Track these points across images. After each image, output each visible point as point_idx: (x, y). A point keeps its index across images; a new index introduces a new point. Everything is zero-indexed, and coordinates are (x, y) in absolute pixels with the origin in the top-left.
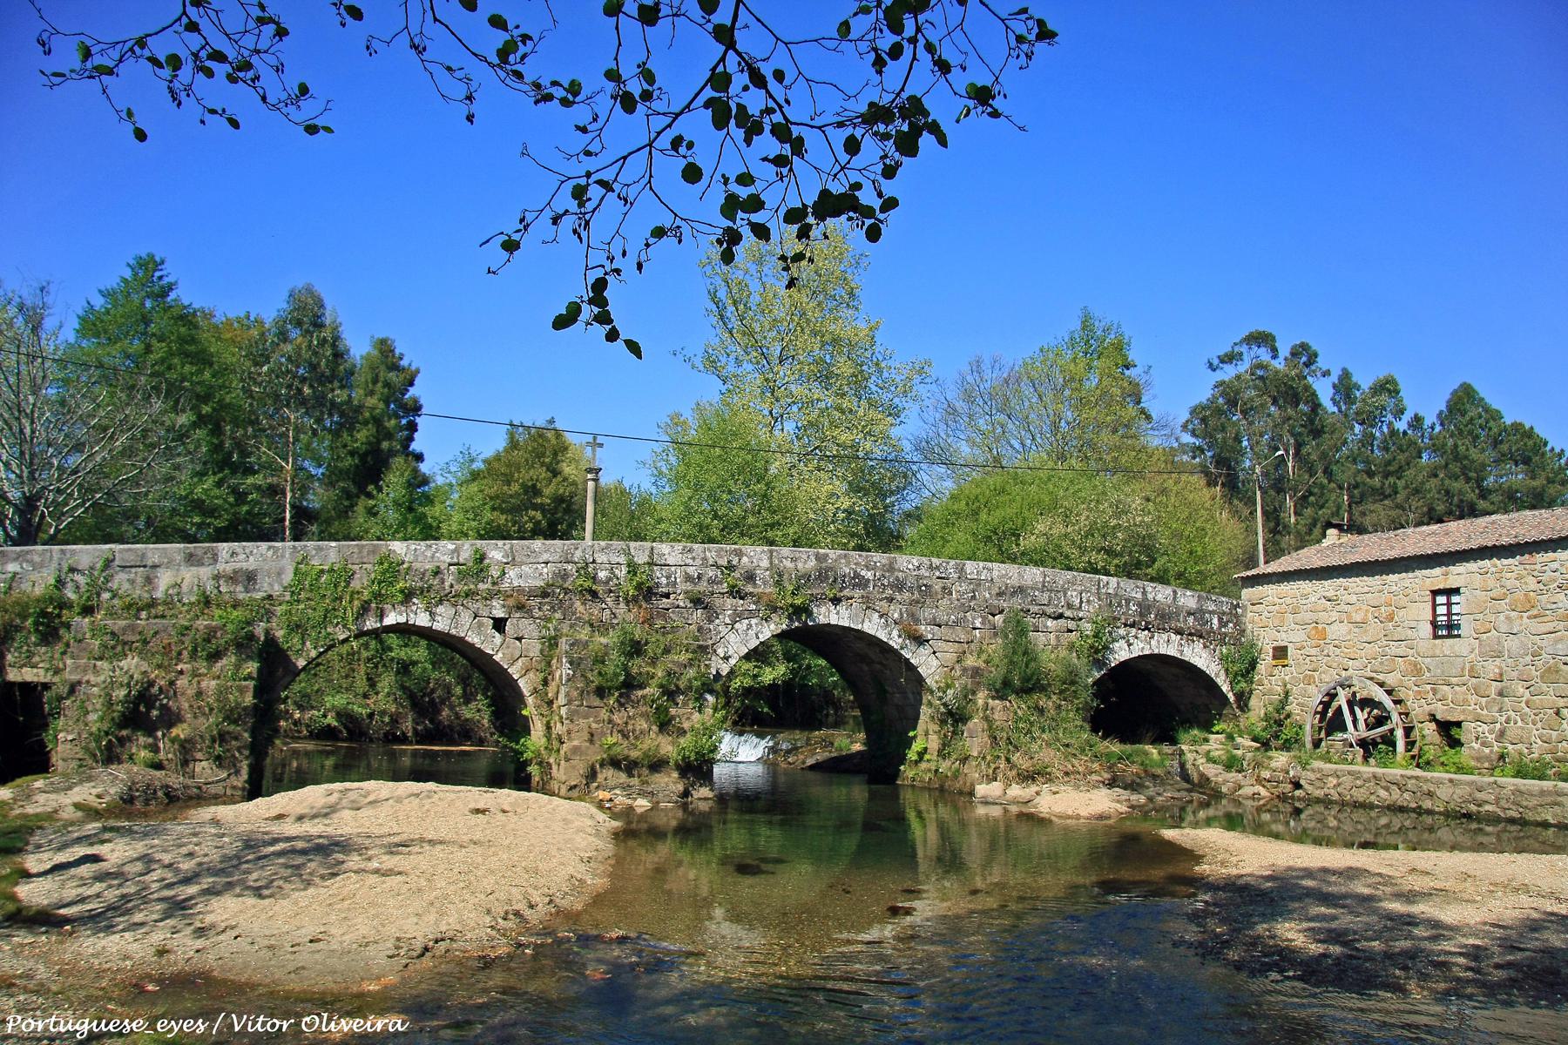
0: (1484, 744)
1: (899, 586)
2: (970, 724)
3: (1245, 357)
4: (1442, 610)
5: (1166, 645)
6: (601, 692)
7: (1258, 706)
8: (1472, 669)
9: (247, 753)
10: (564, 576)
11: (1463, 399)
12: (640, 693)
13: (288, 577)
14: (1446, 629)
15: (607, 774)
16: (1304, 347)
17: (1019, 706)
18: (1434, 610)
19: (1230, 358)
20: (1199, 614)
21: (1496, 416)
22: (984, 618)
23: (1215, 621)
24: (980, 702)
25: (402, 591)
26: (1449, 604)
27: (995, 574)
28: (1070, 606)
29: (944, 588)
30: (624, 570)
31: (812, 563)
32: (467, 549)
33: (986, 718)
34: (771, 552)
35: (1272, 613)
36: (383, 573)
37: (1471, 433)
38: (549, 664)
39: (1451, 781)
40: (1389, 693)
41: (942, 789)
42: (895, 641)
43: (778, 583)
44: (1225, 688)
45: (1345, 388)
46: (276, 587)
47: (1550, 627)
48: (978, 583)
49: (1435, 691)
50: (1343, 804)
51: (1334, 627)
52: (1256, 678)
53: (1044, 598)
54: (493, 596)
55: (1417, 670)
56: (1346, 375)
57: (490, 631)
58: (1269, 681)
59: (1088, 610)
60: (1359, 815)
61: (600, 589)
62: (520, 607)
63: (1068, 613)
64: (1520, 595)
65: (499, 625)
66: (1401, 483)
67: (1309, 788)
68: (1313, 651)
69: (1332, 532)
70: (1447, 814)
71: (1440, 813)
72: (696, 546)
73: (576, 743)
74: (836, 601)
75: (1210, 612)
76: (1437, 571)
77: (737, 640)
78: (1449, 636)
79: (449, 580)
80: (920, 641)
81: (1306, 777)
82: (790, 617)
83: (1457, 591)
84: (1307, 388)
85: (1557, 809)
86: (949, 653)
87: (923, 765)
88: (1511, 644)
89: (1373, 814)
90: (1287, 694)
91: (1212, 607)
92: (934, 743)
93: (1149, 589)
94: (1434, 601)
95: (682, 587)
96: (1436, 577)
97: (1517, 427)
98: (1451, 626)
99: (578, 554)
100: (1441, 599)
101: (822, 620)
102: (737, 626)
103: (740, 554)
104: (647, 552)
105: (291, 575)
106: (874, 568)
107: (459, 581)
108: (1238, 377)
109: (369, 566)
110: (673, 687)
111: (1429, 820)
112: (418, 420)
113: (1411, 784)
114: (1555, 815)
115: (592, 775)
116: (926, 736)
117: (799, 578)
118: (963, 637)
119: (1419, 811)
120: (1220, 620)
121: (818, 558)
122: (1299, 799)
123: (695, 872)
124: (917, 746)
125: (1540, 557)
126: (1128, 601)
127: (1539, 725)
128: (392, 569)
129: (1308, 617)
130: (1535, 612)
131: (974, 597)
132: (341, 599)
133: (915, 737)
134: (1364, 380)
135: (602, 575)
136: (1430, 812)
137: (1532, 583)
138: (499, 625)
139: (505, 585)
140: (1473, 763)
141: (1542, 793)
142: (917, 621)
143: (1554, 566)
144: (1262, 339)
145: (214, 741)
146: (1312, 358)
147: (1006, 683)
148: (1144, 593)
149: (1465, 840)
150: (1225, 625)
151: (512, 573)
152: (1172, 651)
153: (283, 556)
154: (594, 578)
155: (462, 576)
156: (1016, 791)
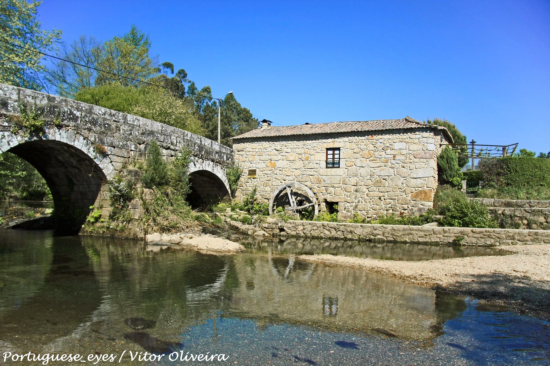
0: (347, 211)
1: (94, 122)
2: (133, 202)
4: (330, 156)
5: (208, 166)
7: (240, 198)
14: (333, 164)
21: (239, 105)
22: (136, 145)
23: (225, 157)
24: (139, 190)
26: (334, 154)
27: (141, 123)
28: (172, 144)
29: (117, 127)
31: (45, 102)
34: (19, 90)
37: (231, 109)
39: (361, 226)
41: (113, 237)
42: (92, 154)
44: (228, 187)
45: (192, 89)
47: (378, 165)
50: (306, 237)
53: (162, 138)
59: (180, 147)
60: (315, 242)
63: (172, 147)
66: (211, 123)
67: (289, 231)
68: (269, 172)
70: (360, 240)
71: (356, 240)
74: (59, 127)
75: (224, 153)
76: (330, 140)
78: (333, 167)
80: (104, 155)
81: (286, 226)
82: (31, 133)
84: (182, 86)
85: (411, 236)
87: (98, 224)
89: (322, 241)
90: (255, 191)
92: (107, 211)
93: (203, 140)
94: (327, 152)
96: (331, 143)
97: (245, 110)
98: (333, 163)
100: (330, 152)
101: (51, 137)
106: (81, 110)
111: (350, 243)
113: (342, 228)
114: (409, 239)
116: (102, 209)
118: (126, 155)
119: (345, 239)
120: (227, 156)
122: (283, 236)
124: (95, 213)
125: (375, 137)
126: (195, 144)
127: (372, 203)
129: (267, 157)
130: (372, 158)
131: (131, 134)
133: (93, 209)
134: (199, 87)
137: (372, 147)
140: (343, 219)
142: (103, 143)
144: (168, 65)
146: (185, 76)
147: (153, 180)
148: (201, 141)
149: (368, 251)
152: (209, 169)
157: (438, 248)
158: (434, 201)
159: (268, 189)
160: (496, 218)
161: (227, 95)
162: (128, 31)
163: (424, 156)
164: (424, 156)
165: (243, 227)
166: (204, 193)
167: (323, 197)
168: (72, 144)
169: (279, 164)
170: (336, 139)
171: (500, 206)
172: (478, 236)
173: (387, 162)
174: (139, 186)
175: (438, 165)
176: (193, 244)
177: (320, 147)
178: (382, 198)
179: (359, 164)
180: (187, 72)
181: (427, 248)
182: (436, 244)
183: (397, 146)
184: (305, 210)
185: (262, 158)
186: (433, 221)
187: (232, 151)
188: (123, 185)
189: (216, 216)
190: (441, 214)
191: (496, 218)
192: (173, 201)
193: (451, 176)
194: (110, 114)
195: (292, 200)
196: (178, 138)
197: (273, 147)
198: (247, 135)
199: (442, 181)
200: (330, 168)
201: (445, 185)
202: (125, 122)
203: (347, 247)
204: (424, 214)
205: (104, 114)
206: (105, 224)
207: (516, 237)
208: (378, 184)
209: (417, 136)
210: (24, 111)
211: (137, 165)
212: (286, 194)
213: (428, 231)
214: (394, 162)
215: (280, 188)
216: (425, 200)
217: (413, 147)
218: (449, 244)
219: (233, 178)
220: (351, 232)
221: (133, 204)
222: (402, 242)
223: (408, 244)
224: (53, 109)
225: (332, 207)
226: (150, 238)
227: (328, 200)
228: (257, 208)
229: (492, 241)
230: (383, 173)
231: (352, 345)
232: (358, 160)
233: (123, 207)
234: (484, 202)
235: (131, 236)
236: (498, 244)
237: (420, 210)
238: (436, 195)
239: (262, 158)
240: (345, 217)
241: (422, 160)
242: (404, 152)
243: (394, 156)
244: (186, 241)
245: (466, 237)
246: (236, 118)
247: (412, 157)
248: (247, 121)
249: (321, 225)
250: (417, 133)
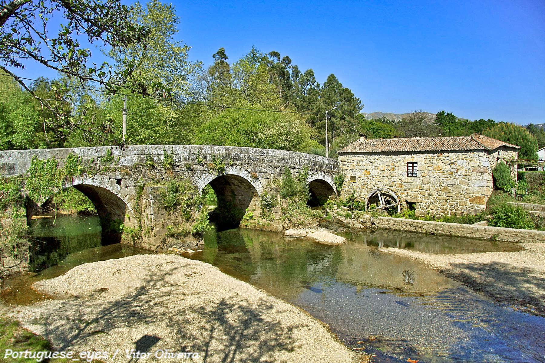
1: (250, 159)
4: (410, 168)
5: (320, 176)
6: (166, 208)
7: (344, 197)
8: (420, 187)
9: (28, 251)
10: (142, 160)
11: (332, 79)
12: (179, 207)
13: (29, 166)
14: (412, 174)
15: (171, 240)
16: (287, 58)
17: (290, 201)
21: (341, 85)
24: (279, 200)
25: (80, 170)
26: (413, 167)
28: (297, 164)
30: (163, 156)
31: (224, 151)
32: (104, 150)
33: (281, 206)
34: (211, 147)
35: (349, 165)
36: (71, 163)
38: (140, 196)
39: (428, 224)
43: (215, 160)
44: (335, 189)
45: (296, 72)
46: (24, 171)
47: (445, 176)
49: (407, 193)
50: (390, 230)
52: (343, 186)
55: (402, 186)
58: (348, 187)
61: (156, 165)
62: (127, 174)
63: (297, 167)
64: (437, 166)
65: (119, 181)
67: (378, 225)
68: (365, 178)
69: (362, 138)
70: (426, 234)
73: (158, 229)
74: (232, 166)
76: (410, 156)
78: (412, 176)
79: (98, 164)
80: (257, 179)
86: (264, 182)
87: (251, 221)
88: (433, 180)
90: (355, 192)
95: (183, 162)
97: (347, 90)
98: (412, 173)
99: (147, 150)
100: (410, 165)
101: (228, 173)
103: (201, 149)
104: (171, 149)
105: (30, 166)
107: (102, 164)
109: (65, 160)
110: (190, 204)
111: (420, 235)
115: (165, 241)
117: (220, 157)
118: (269, 177)
119: (417, 232)
121: (227, 149)
122: (374, 228)
128: (75, 161)
132: (54, 175)
134: (303, 71)
135: (156, 159)
136: (420, 233)
138: (119, 181)
139: (120, 165)
141: (457, 228)
143: (448, 158)
144: (275, 54)
145: (14, 247)
146: (290, 62)
151: (122, 160)
153: (26, 157)
154: (153, 160)
155: (104, 162)
157: (480, 242)
158: (486, 204)
159: (364, 191)
160: (534, 219)
161: (329, 77)
162: (249, 50)
163: (481, 170)
164: (481, 170)
165: (346, 221)
166: (318, 195)
167: (405, 198)
168: (238, 175)
169: (373, 172)
170: (415, 156)
171: (538, 210)
172: (509, 235)
173: (452, 174)
174: (279, 197)
175: (493, 176)
176: (315, 237)
177: (402, 161)
178: (448, 201)
179: (431, 175)
180: (291, 58)
181: (473, 241)
182: (479, 239)
183: (460, 162)
184: (393, 207)
185: (360, 167)
186: (484, 220)
187: (338, 162)
188: (269, 198)
189: (327, 212)
190: (491, 214)
191: (534, 219)
192: (300, 206)
193: (503, 184)
194: (259, 152)
195: (382, 199)
196: (300, 158)
197: (368, 160)
198: (348, 149)
199: (496, 188)
200: (410, 177)
201: (499, 191)
203: (418, 238)
204: (478, 214)
206: (256, 221)
207: (536, 237)
208: (445, 190)
209: (475, 156)
210: (215, 160)
211: (276, 184)
212: (377, 194)
213: (474, 229)
214: (457, 174)
215: (373, 192)
216: (479, 203)
218: (488, 240)
219: (338, 183)
220: (421, 227)
221: (275, 210)
222: (456, 236)
223: (459, 239)
224: (228, 156)
225: (411, 205)
226: (288, 232)
227: (408, 201)
228: (356, 205)
229: (519, 239)
230: (448, 182)
231: (384, 293)
232: (431, 172)
233: (269, 211)
234: (526, 206)
235: (274, 230)
236: (523, 241)
237: (475, 211)
238: (489, 200)
239: (360, 167)
240: (420, 214)
242: (465, 167)
243: (457, 170)
244: (310, 235)
245: (500, 235)
246: (339, 98)
247: (471, 171)
248: (349, 101)
249: (401, 222)
250: (475, 153)
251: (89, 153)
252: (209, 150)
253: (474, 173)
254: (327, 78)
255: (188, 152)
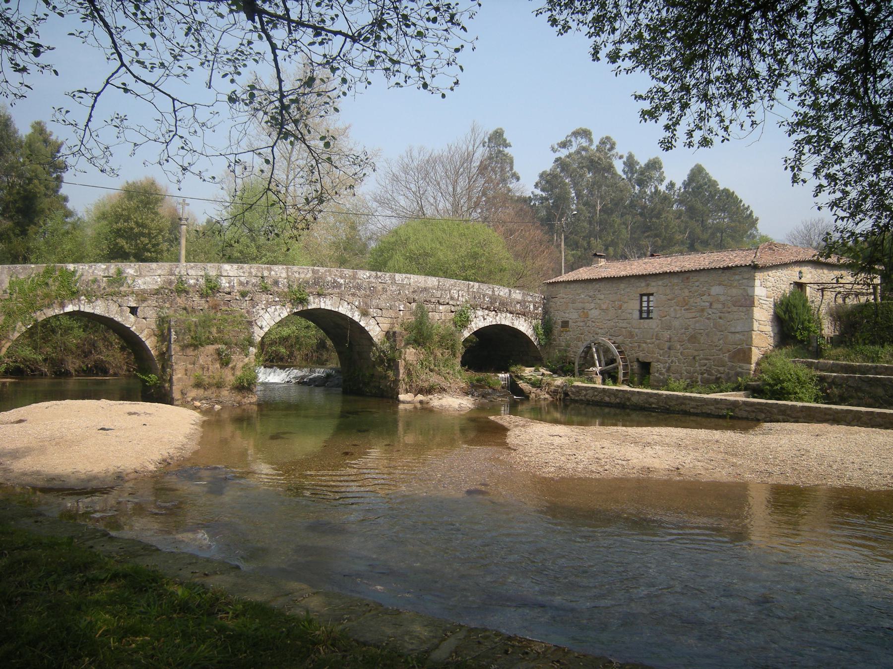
0: (660, 374)
1: (359, 287)
3: (574, 143)
5: (506, 319)
8: (657, 336)
18: (641, 304)
19: (564, 145)
20: (522, 303)
21: (714, 184)
22: (405, 305)
23: (532, 307)
26: (648, 301)
28: (452, 298)
31: (310, 275)
34: (287, 268)
40: (617, 348)
42: (356, 317)
45: (630, 163)
47: (693, 315)
48: (403, 286)
51: (593, 311)
53: (438, 294)
54: (134, 295)
55: (631, 335)
56: (631, 157)
57: (128, 314)
68: (582, 324)
72: (245, 265)
77: (269, 318)
83: (652, 294)
91: (530, 299)
93: (496, 289)
96: (642, 287)
97: (726, 191)
100: (645, 298)
102: (269, 310)
103: (270, 270)
106: (345, 278)
108: (569, 156)
112: (63, 174)
120: (534, 306)
123: (244, 442)
129: (581, 305)
130: (687, 307)
131: (400, 293)
138: (134, 311)
144: (585, 133)
148: (493, 291)
150: (537, 309)
156: (420, 397)
173: (703, 310)
180: (614, 138)
202: (394, 282)
205: (369, 277)
208: (693, 339)
217: (734, 291)
241: (741, 309)
243: (711, 304)
251: (91, 271)
252: (284, 271)
253: (735, 309)
254: (688, 172)
255: (247, 274)
